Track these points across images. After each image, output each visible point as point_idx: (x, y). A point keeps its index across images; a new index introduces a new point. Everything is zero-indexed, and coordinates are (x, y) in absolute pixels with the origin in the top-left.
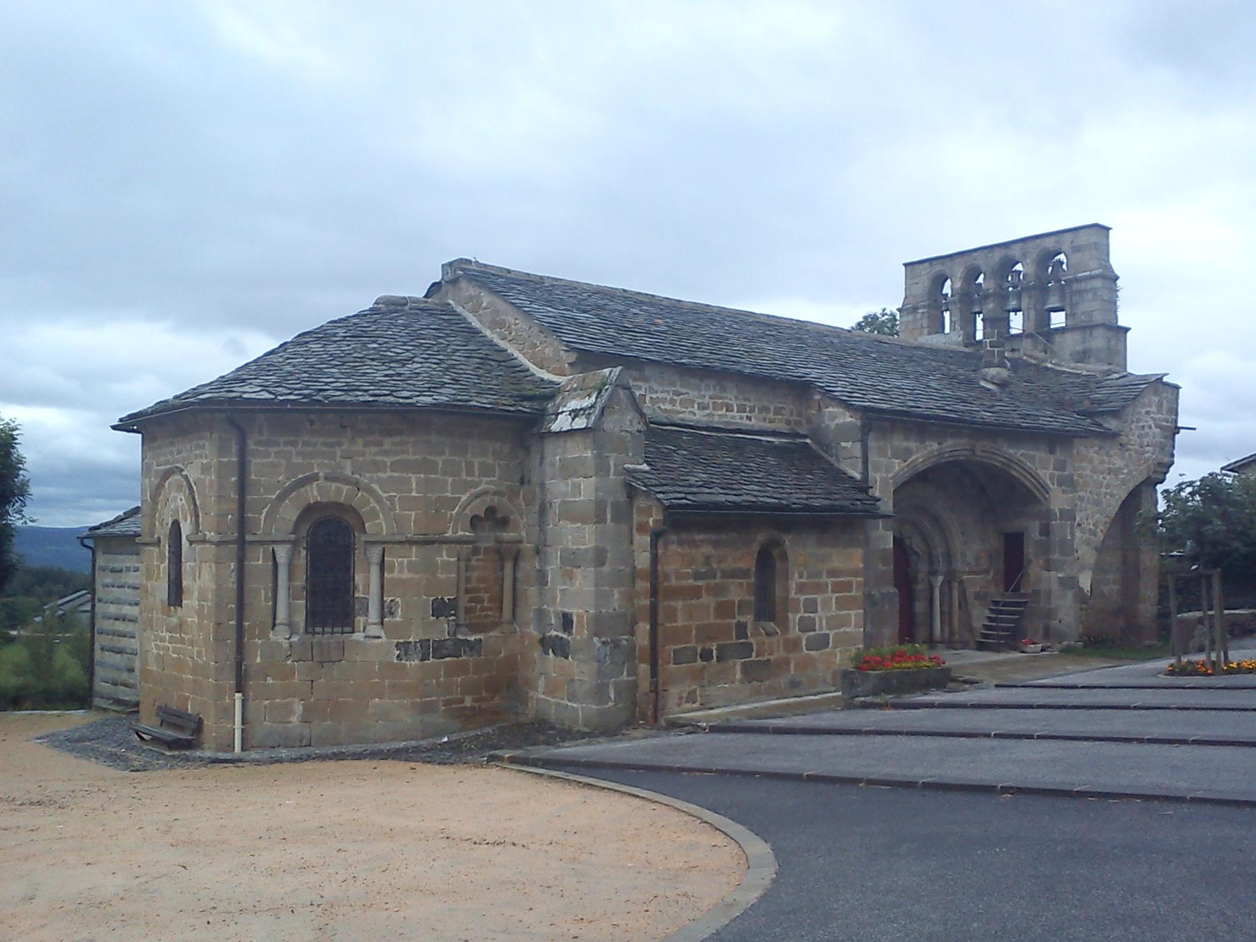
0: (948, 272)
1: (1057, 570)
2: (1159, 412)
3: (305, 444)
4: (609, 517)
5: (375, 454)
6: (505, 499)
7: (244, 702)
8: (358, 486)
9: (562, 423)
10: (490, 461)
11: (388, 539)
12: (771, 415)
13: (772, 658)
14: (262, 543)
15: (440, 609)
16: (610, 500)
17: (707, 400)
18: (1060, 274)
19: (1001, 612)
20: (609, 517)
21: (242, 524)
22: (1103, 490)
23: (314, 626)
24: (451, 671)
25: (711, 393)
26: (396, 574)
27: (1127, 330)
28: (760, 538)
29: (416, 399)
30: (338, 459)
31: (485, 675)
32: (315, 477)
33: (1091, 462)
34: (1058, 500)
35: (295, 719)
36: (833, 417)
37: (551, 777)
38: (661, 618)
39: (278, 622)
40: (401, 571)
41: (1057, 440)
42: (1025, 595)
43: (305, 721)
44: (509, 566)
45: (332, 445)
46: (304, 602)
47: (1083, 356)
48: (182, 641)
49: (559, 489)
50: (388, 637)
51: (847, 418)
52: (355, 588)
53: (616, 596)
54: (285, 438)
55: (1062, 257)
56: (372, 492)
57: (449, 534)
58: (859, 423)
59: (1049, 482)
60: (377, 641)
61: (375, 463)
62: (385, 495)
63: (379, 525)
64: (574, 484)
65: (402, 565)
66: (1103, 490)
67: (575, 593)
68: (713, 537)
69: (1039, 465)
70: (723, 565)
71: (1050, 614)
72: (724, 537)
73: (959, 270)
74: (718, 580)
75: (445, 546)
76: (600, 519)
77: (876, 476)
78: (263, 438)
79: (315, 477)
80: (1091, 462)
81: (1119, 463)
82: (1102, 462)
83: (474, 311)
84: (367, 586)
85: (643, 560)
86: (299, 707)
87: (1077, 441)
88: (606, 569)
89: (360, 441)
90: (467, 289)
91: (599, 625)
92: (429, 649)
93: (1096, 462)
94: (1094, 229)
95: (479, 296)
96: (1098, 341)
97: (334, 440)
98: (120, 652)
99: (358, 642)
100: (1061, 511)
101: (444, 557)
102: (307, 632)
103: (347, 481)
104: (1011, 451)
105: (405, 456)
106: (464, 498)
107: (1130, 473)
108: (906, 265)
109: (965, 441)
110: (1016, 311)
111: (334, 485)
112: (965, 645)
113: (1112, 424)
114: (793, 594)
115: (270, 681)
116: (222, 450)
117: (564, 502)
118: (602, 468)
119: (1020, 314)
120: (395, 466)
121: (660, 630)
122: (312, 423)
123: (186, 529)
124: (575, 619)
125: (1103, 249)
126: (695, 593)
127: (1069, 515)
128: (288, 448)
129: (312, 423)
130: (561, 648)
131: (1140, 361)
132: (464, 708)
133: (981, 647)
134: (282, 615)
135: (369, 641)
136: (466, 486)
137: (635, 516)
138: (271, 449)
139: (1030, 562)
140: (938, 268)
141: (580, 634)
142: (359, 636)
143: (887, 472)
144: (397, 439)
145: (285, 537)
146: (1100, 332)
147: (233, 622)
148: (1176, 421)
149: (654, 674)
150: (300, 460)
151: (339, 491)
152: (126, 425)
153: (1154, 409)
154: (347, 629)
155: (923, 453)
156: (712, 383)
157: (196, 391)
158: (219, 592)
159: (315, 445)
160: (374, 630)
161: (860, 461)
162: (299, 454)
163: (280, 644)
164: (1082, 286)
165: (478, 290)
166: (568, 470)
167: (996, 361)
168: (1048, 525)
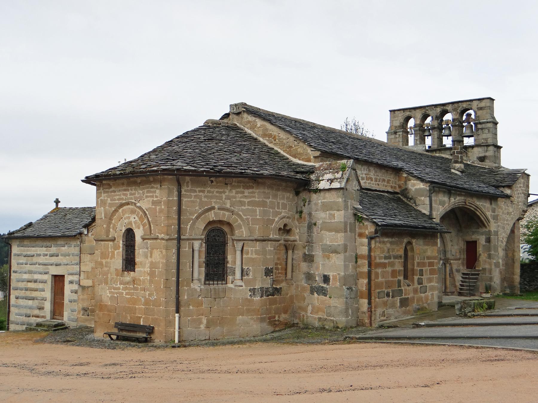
0: (413, 115)
1: (493, 259)
2: (524, 187)
3: (208, 192)
4: (348, 229)
5: (241, 198)
6: (290, 220)
7: (179, 317)
8: (233, 212)
9: (323, 185)
10: (285, 202)
11: (247, 238)
12: (386, 184)
13: (409, 296)
14: (188, 239)
15: (268, 272)
16: (349, 221)
17: (364, 176)
18: (473, 118)
19: (466, 278)
20: (348, 229)
21: (179, 231)
22: (505, 222)
23: (208, 280)
24: (272, 303)
25: (365, 172)
26: (249, 256)
27: (501, 147)
28: (405, 240)
29: (246, 171)
30: (223, 199)
31: (283, 305)
32: (213, 208)
33: (502, 209)
34: (493, 226)
35: (202, 327)
36: (414, 185)
37: (395, 343)
38: (373, 277)
39: (194, 278)
40: (252, 254)
41: (493, 198)
42: (479, 271)
43: (207, 327)
44: (290, 252)
45: (221, 193)
46: (204, 269)
47: (482, 159)
48: (136, 289)
49: (321, 216)
50: (246, 286)
51: (421, 185)
52: (227, 262)
53: (351, 267)
54: (199, 189)
55: (471, 112)
56: (239, 216)
57: (271, 236)
58: (428, 188)
59: (490, 218)
60: (241, 288)
61: (240, 201)
62: (245, 217)
63: (242, 232)
64: (330, 214)
65: (253, 251)
66: (505, 222)
67: (334, 266)
68: (390, 240)
69: (485, 208)
70: (394, 253)
71: (491, 279)
72: (394, 240)
73: (419, 114)
74: (392, 260)
75: (269, 242)
76: (346, 231)
77: (434, 213)
78: (189, 188)
79: (213, 208)
80: (502, 209)
81: (511, 210)
82: (506, 209)
83: (252, 128)
84: (234, 262)
85: (364, 250)
86: (205, 321)
87: (499, 199)
88: (347, 254)
89: (234, 191)
90: (247, 117)
91: (345, 280)
92: (265, 292)
93: (504, 209)
94: (489, 100)
95: (255, 121)
96: (491, 151)
97: (222, 190)
98: (33, 299)
99: (232, 288)
100: (494, 231)
101: (269, 247)
102: (205, 284)
103: (227, 210)
104: (478, 203)
105: (253, 199)
106: (276, 219)
107: (514, 215)
108: (391, 111)
109: (463, 198)
110: (428, 136)
111: (222, 212)
112: (452, 293)
113: (508, 191)
114: (415, 268)
115: (191, 308)
116: (170, 193)
117: (324, 222)
118: (346, 208)
119: (430, 137)
120: (250, 203)
121: (373, 283)
122: (212, 182)
123: (139, 234)
124: (331, 277)
125: (491, 108)
126: (384, 265)
127: (496, 233)
128: (201, 194)
129: (212, 182)
130: (322, 291)
131: (509, 161)
132: (275, 321)
133: (460, 294)
134: (196, 275)
135: (236, 288)
136: (277, 214)
137: (357, 229)
138: (193, 194)
139: (480, 255)
140: (408, 113)
141: (335, 284)
142: (230, 285)
143: (437, 212)
144: (250, 190)
145: (199, 237)
146: (491, 148)
147: (174, 279)
148: (528, 191)
149: (370, 303)
150: (206, 200)
151: (224, 215)
152: (88, 180)
153: (522, 185)
154: (223, 282)
155: (455, 201)
156: (366, 167)
157: (129, 164)
158: (167, 264)
159: (213, 192)
160: (240, 283)
161: (429, 206)
162: (205, 197)
163: (196, 290)
164: (483, 126)
165: (254, 118)
166: (326, 207)
167: (460, 160)
168: (490, 237)
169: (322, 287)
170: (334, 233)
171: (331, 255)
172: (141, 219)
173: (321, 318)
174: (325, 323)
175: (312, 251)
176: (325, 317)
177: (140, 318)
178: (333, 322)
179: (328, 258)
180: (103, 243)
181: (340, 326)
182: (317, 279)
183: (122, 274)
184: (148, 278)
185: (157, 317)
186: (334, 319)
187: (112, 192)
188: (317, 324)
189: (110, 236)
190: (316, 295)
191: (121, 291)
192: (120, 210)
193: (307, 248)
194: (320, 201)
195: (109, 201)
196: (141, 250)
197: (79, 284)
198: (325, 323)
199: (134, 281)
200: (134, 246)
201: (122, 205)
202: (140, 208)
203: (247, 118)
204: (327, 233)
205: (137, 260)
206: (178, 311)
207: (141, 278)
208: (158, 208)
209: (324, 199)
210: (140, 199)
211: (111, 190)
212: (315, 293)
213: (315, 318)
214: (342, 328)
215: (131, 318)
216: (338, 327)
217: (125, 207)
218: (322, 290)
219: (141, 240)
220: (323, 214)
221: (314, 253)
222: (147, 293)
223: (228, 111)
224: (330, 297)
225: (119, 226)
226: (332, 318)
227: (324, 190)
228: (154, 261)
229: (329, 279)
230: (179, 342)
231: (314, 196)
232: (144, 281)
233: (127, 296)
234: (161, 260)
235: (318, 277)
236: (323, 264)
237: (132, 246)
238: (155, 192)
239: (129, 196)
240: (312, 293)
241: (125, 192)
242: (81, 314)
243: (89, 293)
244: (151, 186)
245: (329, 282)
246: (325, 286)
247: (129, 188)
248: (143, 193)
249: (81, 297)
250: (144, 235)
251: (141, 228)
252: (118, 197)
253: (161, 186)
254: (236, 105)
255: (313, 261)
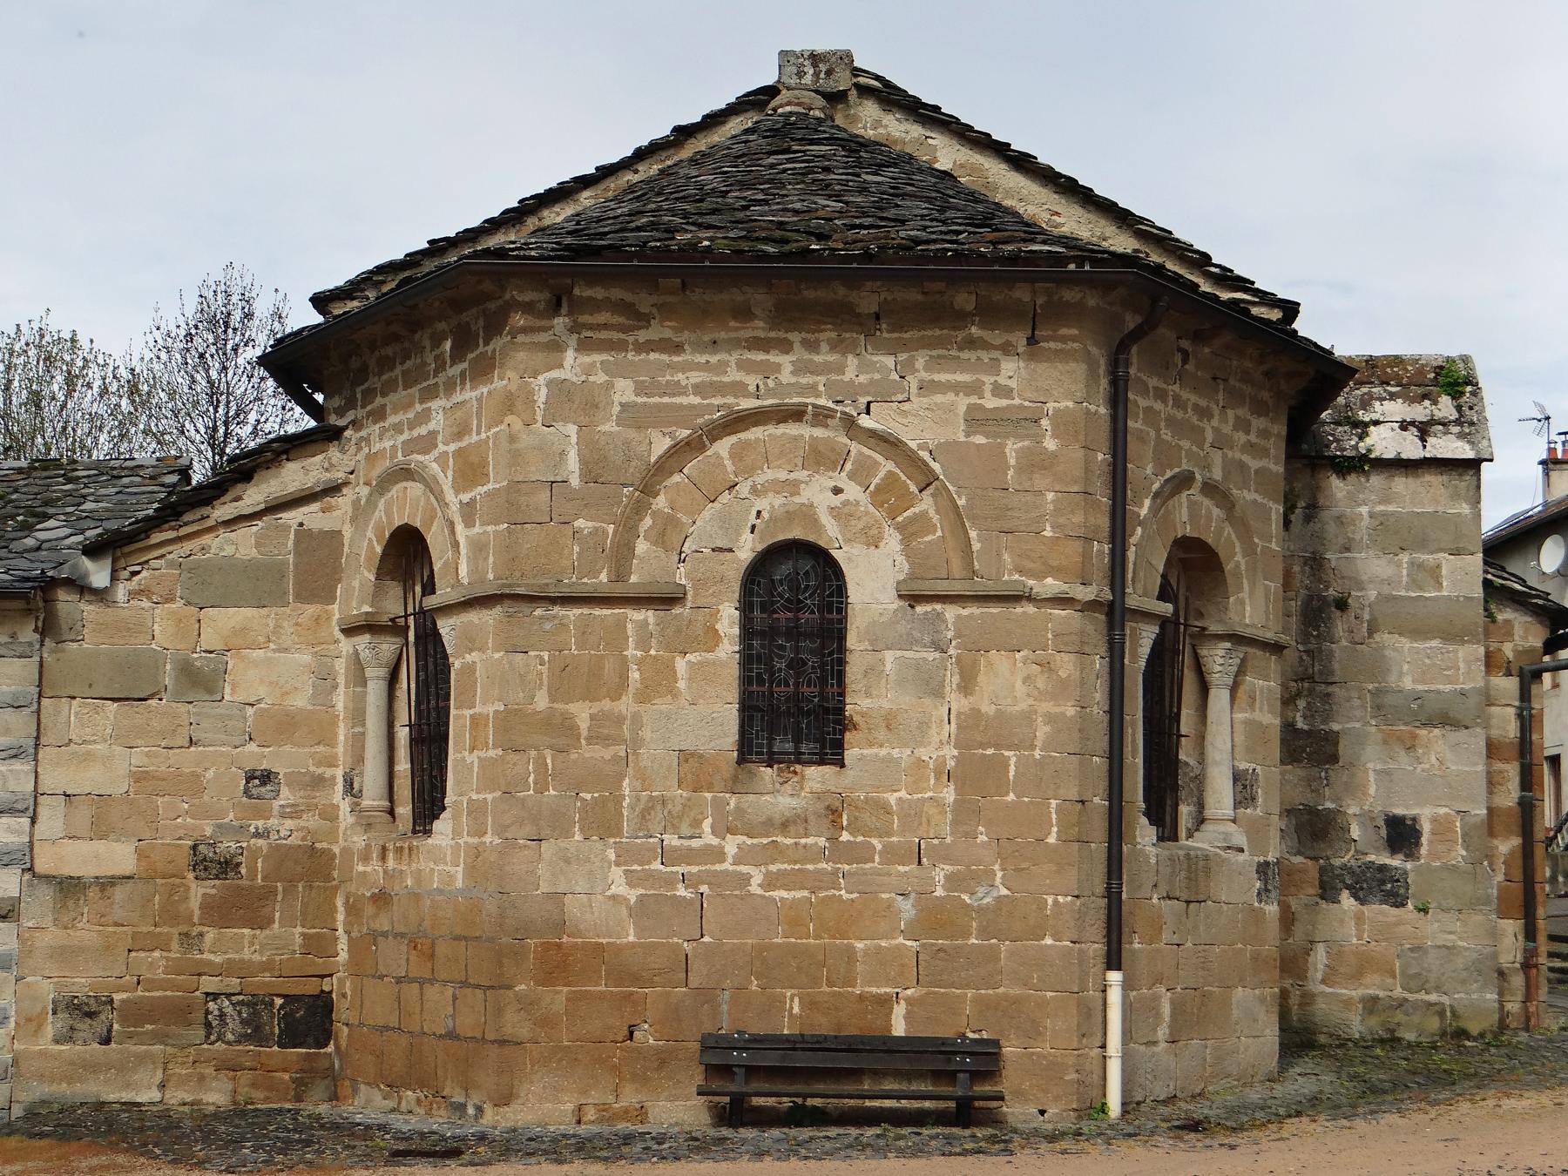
9: (1384, 442)
30: (1207, 445)
49: (1375, 573)
64: (1416, 566)
124: (1426, 827)
130: (1381, 886)
169: (1383, 868)
170: (1435, 643)
171: (1423, 732)
172: (888, 497)
173: (1375, 999)
174: (1399, 1017)
175: (1327, 718)
176: (1398, 992)
177: (886, 1003)
178: (1442, 1014)
179: (1410, 749)
180: (574, 612)
181: (1474, 1029)
182: (1355, 832)
183: (735, 779)
184: (949, 794)
185: (1016, 991)
186: (1445, 1000)
187: (649, 346)
188: (1356, 1025)
189: (633, 579)
190: (1347, 901)
191: (727, 866)
192: (723, 447)
193: (1301, 704)
194: (1364, 510)
195: (624, 391)
196: (889, 656)
197: (31, 869)
198: (1399, 1017)
199: (834, 813)
200: (841, 636)
201: (737, 422)
202: (887, 443)
203: (877, 124)
204: (1405, 644)
205: (857, 703)
206: (1114, 961)
207: (892, 798)
208: (1012, 448)
209: (1385, 500)
210: (884, 394)
211: (642, 336)
212: (1345, 894)
213: (1348, 1003)
214: (1482, 1035)
215: (810, 1004)
216: (1462, 1033)
217: (754, 433)
218: (1383, 882)
219: (893, 604)
220: (1383, 561)
221: (1336, 727)
222: (939, 874)
223: (770, 79)
224: (1424, 910)
225: (704, 527)
226: (1433, 997)
227: (1401, 465)
228: (987, 709)
229: (1417, 834)
230: (1125, 1112)
231: (1338, 488)
232: (912, 815)
233: (779, 894)
234: (1047, 707)
235: (1362, 825)
236: (1383, 774)
237: (771, 633)
238: (994, 367)
239: (786, 376)
240: (1328, 892)
241: (760, 356)
242: (49, 1031)
243: (118, 914)
244: (961, 335)
245: (1418, 844)
246: (1396, 862)
247: (795, 337)
248: (910, 366)
249: (52, 936)
250: (912, 577)
251: (892, 541)
252: (696, 377)
253: (1032, 341)
254: (815, 58)
255: (1334, 758)
